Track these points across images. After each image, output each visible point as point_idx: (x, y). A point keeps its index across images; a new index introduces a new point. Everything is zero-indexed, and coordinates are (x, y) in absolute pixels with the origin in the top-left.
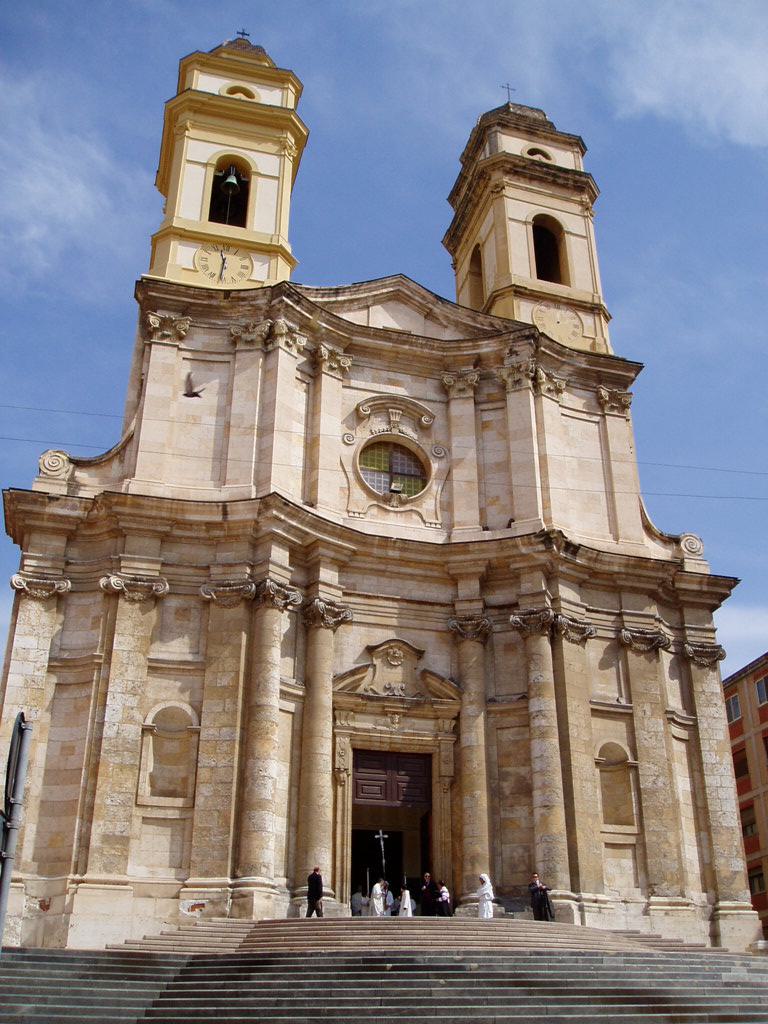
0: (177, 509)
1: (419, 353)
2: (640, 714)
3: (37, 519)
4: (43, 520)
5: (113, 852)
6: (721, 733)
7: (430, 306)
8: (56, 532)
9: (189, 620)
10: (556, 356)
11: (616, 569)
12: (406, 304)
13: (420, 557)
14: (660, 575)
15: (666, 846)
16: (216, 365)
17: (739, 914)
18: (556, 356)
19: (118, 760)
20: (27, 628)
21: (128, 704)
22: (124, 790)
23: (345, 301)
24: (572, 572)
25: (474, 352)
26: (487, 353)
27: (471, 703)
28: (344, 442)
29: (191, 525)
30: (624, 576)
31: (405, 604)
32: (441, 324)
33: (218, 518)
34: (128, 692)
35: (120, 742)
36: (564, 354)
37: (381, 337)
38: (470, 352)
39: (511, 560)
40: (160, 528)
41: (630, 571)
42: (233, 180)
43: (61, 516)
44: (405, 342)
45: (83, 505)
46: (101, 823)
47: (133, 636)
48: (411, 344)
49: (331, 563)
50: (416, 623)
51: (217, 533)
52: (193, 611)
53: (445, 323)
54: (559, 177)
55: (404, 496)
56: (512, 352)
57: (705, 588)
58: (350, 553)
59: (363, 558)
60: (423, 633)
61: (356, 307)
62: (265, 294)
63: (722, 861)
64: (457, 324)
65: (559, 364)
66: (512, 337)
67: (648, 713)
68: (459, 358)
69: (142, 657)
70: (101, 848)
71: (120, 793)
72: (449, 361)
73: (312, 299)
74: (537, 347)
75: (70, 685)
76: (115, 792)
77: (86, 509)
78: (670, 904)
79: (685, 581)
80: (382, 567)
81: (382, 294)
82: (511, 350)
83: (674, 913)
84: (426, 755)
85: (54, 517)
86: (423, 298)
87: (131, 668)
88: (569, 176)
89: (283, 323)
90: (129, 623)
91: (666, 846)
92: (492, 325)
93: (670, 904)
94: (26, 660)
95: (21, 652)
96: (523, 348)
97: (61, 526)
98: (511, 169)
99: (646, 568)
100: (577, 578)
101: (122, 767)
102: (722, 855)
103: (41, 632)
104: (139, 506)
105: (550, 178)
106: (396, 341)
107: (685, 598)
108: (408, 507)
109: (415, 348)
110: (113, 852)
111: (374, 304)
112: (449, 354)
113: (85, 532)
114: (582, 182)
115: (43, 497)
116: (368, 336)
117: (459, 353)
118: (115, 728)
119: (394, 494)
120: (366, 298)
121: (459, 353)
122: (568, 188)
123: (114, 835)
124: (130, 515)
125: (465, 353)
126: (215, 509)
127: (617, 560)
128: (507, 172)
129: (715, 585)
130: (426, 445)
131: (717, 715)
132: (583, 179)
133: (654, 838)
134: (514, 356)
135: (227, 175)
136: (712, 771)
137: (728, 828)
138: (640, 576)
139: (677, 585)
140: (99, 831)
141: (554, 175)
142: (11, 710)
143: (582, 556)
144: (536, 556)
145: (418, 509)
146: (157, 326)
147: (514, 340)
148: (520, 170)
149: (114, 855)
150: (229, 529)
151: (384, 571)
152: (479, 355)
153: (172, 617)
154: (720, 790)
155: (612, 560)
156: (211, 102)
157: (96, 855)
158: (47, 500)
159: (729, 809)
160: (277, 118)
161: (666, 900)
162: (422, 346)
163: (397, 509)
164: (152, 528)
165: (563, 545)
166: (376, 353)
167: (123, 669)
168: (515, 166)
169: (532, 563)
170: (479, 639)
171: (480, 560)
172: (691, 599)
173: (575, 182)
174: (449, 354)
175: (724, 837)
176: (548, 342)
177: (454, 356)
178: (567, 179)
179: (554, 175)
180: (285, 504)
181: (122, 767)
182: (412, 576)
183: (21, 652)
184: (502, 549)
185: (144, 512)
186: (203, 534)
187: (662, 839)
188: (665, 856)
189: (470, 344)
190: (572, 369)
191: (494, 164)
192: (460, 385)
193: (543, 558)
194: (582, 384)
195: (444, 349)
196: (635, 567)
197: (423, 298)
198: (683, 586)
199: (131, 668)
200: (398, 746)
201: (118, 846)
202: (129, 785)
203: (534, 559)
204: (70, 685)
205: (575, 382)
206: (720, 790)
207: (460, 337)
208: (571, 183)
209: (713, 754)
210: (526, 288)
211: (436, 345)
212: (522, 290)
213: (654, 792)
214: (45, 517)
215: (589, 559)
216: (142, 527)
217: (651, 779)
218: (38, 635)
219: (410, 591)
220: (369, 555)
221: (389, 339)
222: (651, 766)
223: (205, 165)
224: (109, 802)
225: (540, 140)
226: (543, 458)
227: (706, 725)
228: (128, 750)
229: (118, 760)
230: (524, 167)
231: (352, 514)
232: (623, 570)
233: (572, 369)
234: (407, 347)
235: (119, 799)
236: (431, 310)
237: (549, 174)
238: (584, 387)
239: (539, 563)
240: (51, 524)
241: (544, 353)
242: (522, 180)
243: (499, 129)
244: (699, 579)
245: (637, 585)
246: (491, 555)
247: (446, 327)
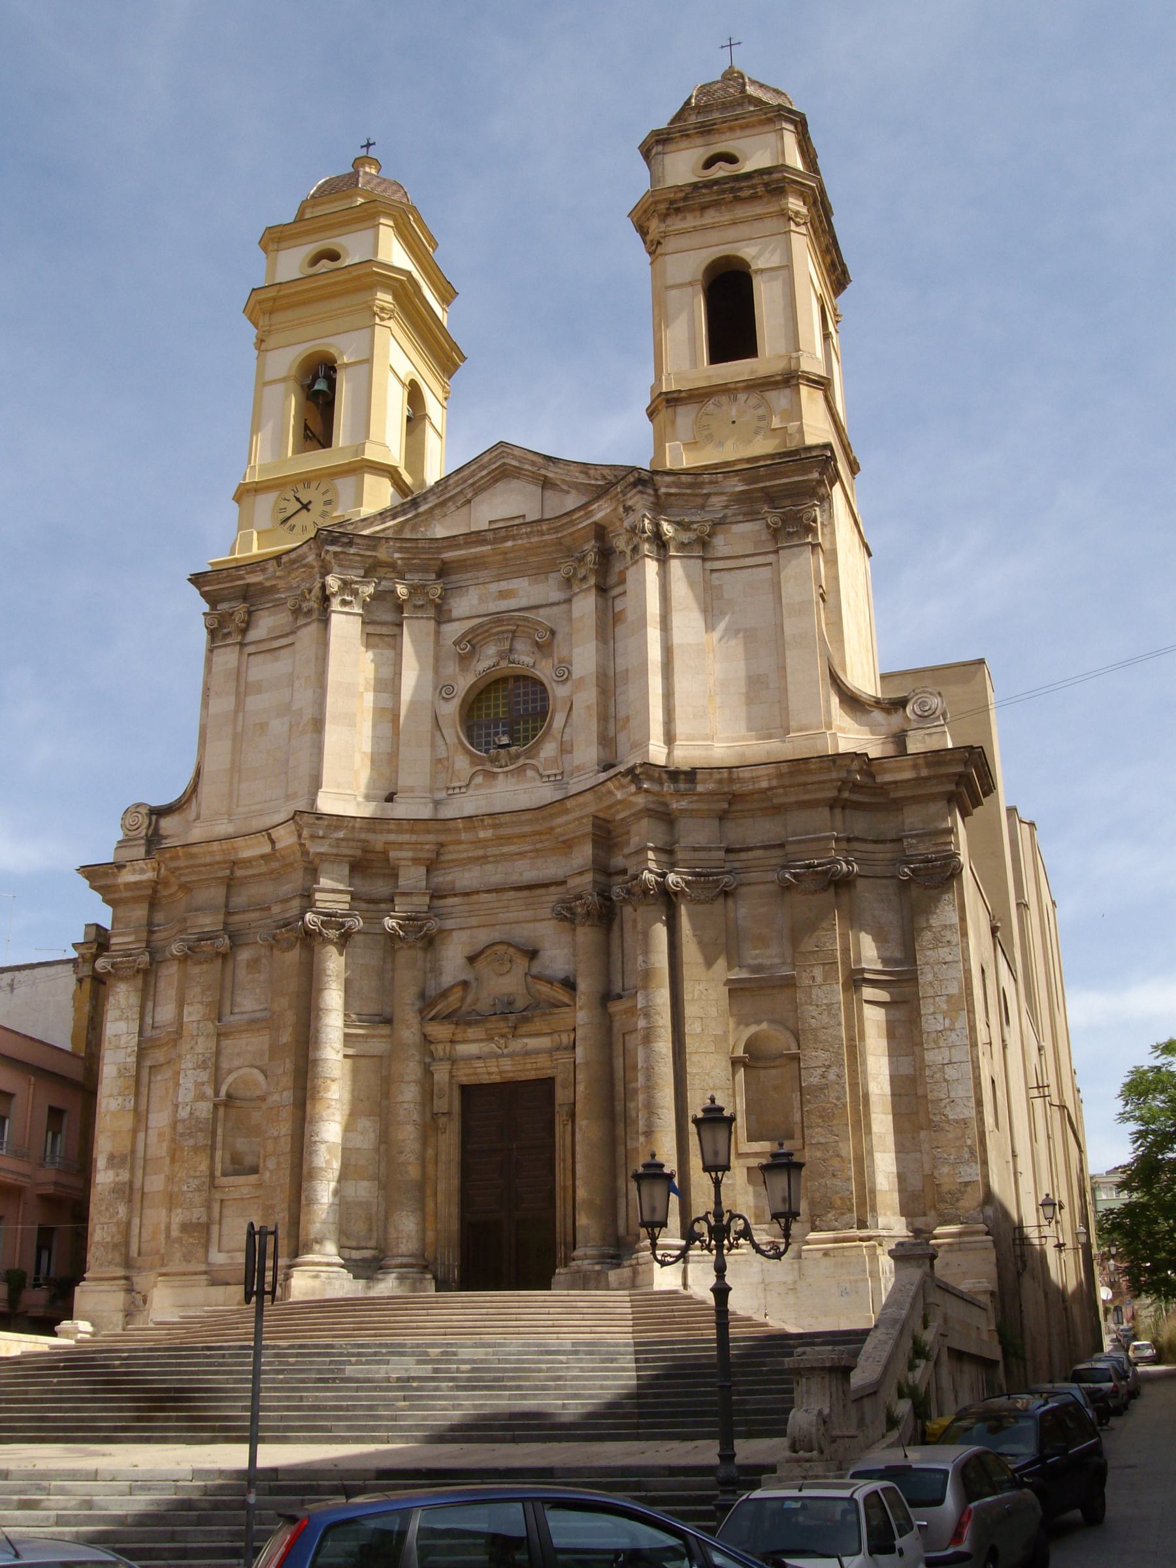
0: (205, 853)
1: (528, 545)
2: (807, 982)
3: (115, 892)
4: (121, 891)
5: (191, 1240)
6: (955, 984)
7: (543, 472)
8: (136, 900)
9: (259, 972)
10: (688, 491)
11: (764, 784)
12: (518, 478)
13: (517, 830)
14: (834, 775)
15: (835, 1162)
16: (282, 651)
17: (843, 1248)
18: (688, 491)
19: (191, 1142)
20: (117, 1013)
21: (199, 1080)
22: (198, 1174)
23: (432, 509)
24: (695, 806)
25: (589, 522)
26: (603, 518)
27: (581, 1008)
28: (444, 698)
29: (250, 862)
30: (781, 791)
31: (512, 893)
32: (562, 491)
33: (267, 849)
34: (198, 1067)
35: (193, 1122)
36: (703, 483)
37: (474, 542)
38: (585, 524)
39: (613, 810)
40: (220, 874)
41: (787, 781)
42: (321, 385)
43: (135, 883)
44: (505, 539)
45: (149, 866)
46: (179, 1211)
47: (201, 1003)
48: (514, 538)
49: (414, 864)
50: (529, 914)
51: (275, 865)
52: (264, 961)
53: (565, 487)
54: (741, 189)
55: (513, 749)
56: (628, 509)
57: (924, 773)
58: (433, 847)
59: (457, 848)
60: (538, 925)
61: (453, 508)
62: (311, 548)
63: (945, 1170)
64: (576, 486)
65: (700, 501)
66: (619, 490)
67: (819, 980)
68: (577, 535)
69: (211, 1025)
70: (181, 1238)
71: (195, 1177)
72: (568, 541)
73: (365, 533)
74: (656, 490)
75: (161, 1065)
76: (190, 1177)
77: (154, 869)
78: (836, 1241)
79: (890, 771)
80: (480, 853)
81: (483, 477)
82: (624, 507)
83: (836, 1253)
84: (550, 1078)
85: (130, 886)
86: (533, 463)
87: (201, 1040)
88: (754, 181)
89: (333, 583)
90: (198, 990)
91: (835, 1162)
92: (604, 478)
93: (836, 1241)
94: (118, 1047)
95: (113, 1039)
96: (635, 499)
97: (138, 893)
98: (668, 209)
99: (810, 772)
100: (709, 810)
101: (196, 1149)
102: (945, 1161)
103: (129, 1014)
104: (192, 856)
105: (730, 196)
106: (495, 541)
107: (900, 794)
108: (521, 761)
109: (520, 542)
110: (191, 1240)
111: (476, 494)
112: (565, 533)
113: (165, 893)
114: (778, 181)
115: (111, 868)
116: (458, 547)
117: (575, 528)
118: (188, 1108)
119: (502, 751)
120: (461, 492)
121: (575, 528)
122: (761, 197)
123: (191, 1223)
124: (187, 867)
125: (580, 526)
126: (262, 838)
127: (762, 771)
128: (664, 217)
129: (939, 763)
130: (544, 671)
131: (949, 958)
132: (776, 176)
133: (819, 1154)
134: (631, 513)
135: (315, 378)
136: (936, 1041)
137: (957, 1121)
138: (805, 784)
139: (880, 779)
140: (177, 1220)
141: (732, 190)
142: (108, 1103)
143: (704, 782)
144: (632, 799)
145: (533, 762)
146: (216, 626)
147: (624, 493)
148: (681, 204)
149: (192, 1243)
150: (283, 857)
151: (485, 857)
152: (596, 524)
153: (244, 972)
154: (948, 1069)
155: (754, 774)
156: (281, 293)
157: (176, 1245)
158: (116, 870)
159: (961, 1093)
160: (359, 277)
161: (830, 1235)
162: (528, 535)
163: (506, 769)
164: (212, 876)
165: (665, 776)
166: (477, 564)
167: (193, 1042)
168: (672, 202)
169: (633, 811)
170: (588, 923)
171: (582, 817)
172: (909, 793)
173: (766, 185)
174: (565, 533)
175: (950, 1136)
176: (668, 479)
177: (571, 534)
178: (753, 187)
179: (732, 190)
180: (318, 819)
181: (196, 1149)
182: (521, 855)
183: (113, 1039)
184: (600, 798)
185: (198, 861)
186: (263, 869)
187: (831, 1153)
188: (834, 1175)
189: (582, 513)
190: (725, 498)
191: (645, 212)
192: (582, 572)
193: (641, 800)
194: (744, 514)
195: (556, 530)
196: (791, 774)
197: (533, 463)
198: (888, 778)
199: (201, 1040)
200: (511, 1075)
201: (196, 1234)
202: (204, 1167)
203: (633, 804)
204: (161, 1065)
205: (734, 515)
206: (948, 1069)
207: (584, 500)
208: (760, 190)
209: (940, 1017)
210: (680, 391)
211: (545, 528)
212: (675, 395)
213: (822, 1088)
214: (121, 887)
215: (720, 781)
216: (203, 877)
217: (819, 1071)
218: (127, 1018)
219: (521, 874)
220: (460, 842)
221: (485, 542)
222: (820, 1053)
223: (691, 284)
224: (185, 1188)
225: (724, 137)
226: (238, 795)
227: (930, 977)
228: (201, 1130)
229: (191, 1142)
230: (685, 199)
231: (451, 792)
232: (774, 783)
233: (725, 498)
234: (509, 544)
235: (194, 1183)
236: (546, 477)
237: (723, 192)
238: (750, 518)
239: (639, 808)
240: (129, 894)
241: (669, 495)
242: (689, 216)
243: (660, 148)
244: (910, 763)
245: (806, 797)
246: (591, 809)
247: (568, 492)
